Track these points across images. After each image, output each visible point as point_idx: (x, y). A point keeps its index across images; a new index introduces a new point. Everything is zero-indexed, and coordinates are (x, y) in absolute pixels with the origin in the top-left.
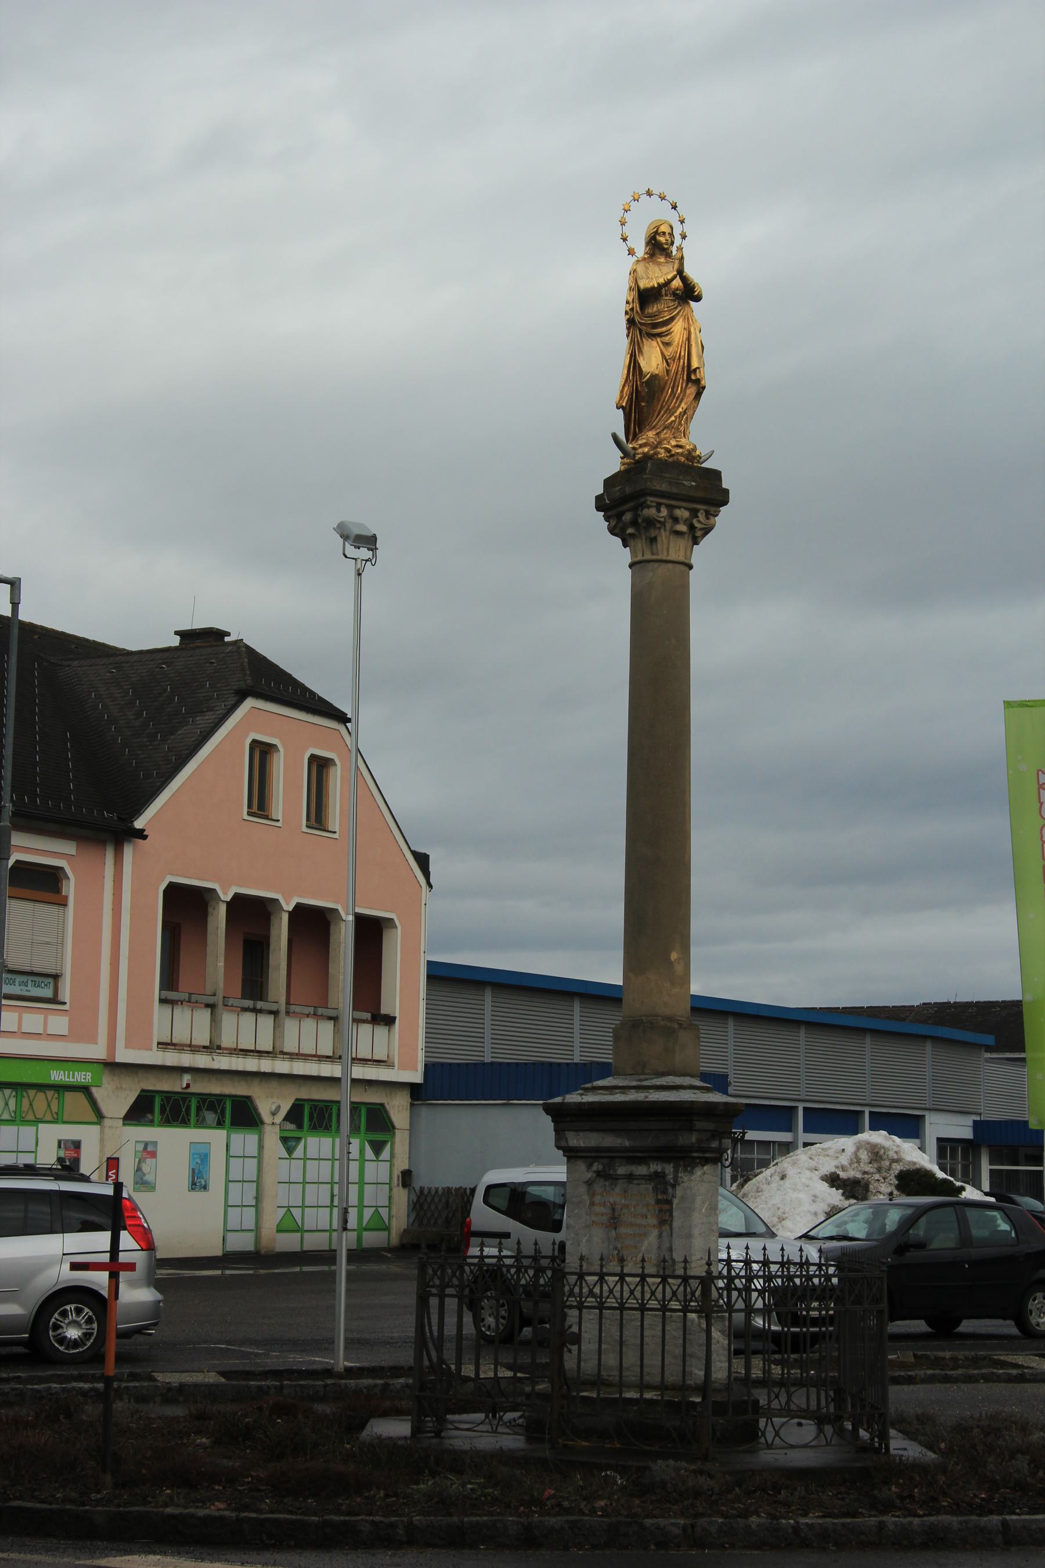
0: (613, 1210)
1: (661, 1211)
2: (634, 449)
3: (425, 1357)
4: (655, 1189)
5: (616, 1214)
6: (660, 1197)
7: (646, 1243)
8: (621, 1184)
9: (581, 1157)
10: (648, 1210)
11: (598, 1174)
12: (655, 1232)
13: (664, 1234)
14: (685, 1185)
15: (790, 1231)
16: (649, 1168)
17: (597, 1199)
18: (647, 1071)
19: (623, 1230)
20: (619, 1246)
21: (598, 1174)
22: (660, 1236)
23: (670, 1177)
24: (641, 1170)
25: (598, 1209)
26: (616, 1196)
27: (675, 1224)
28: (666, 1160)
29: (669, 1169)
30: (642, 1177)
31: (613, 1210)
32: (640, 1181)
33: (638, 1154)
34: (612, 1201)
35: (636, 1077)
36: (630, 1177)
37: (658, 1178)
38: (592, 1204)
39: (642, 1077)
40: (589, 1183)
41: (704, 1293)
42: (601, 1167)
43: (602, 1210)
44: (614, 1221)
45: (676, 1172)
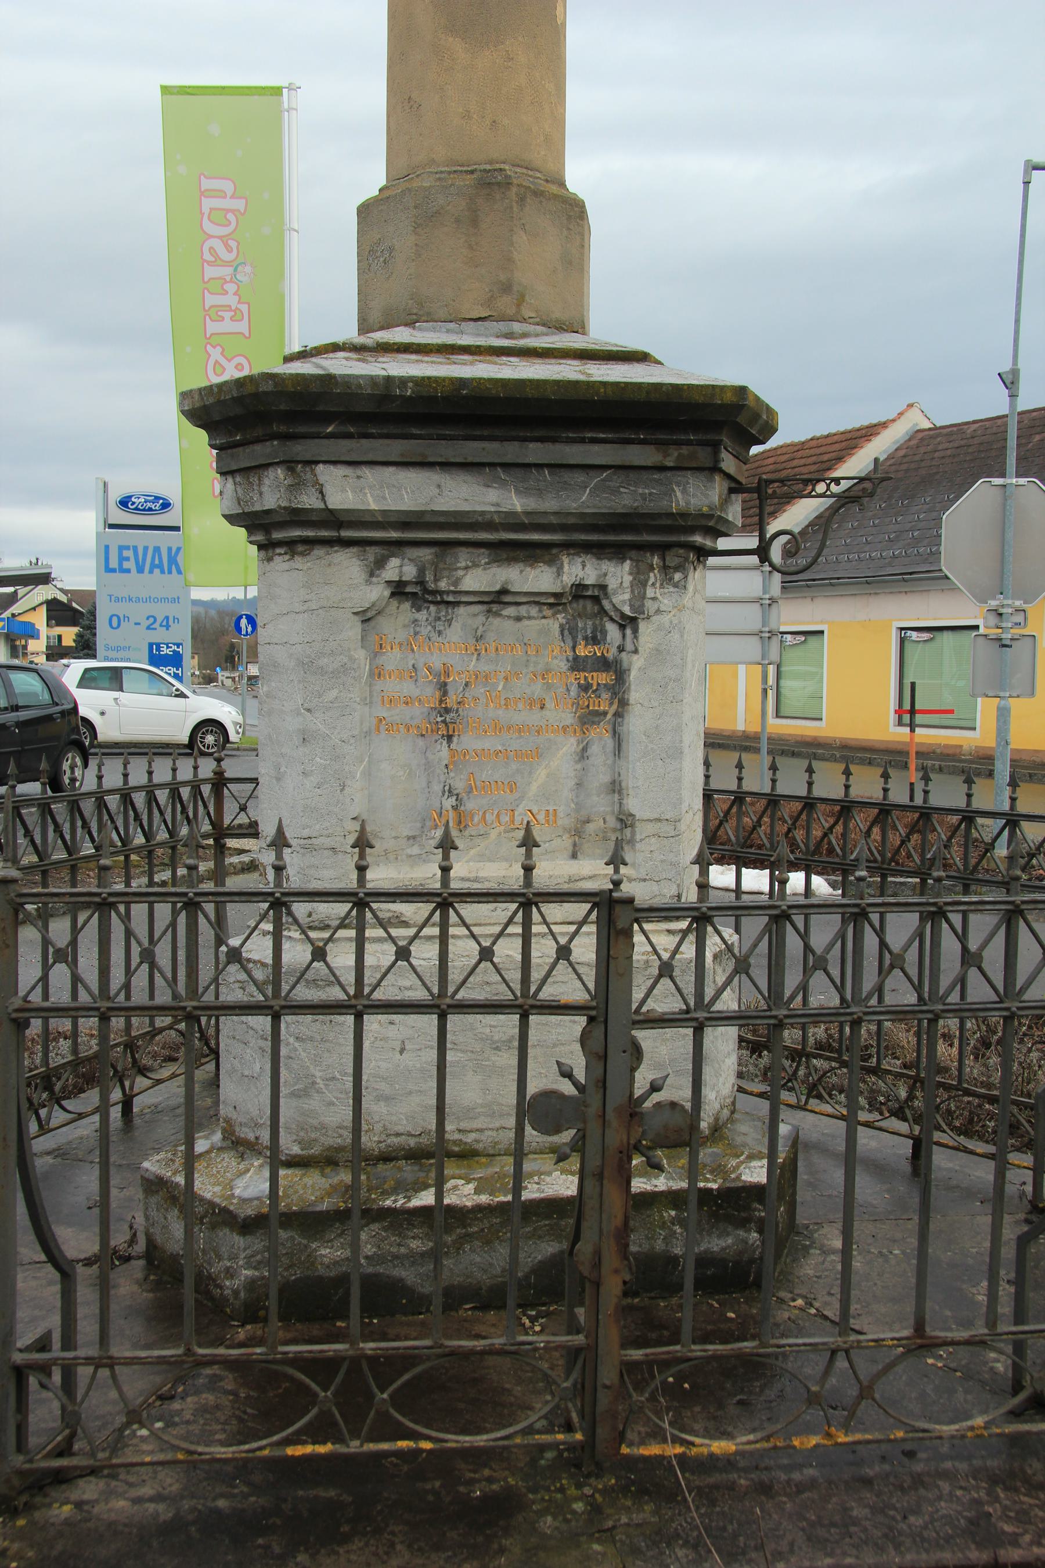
0: (443, 687)
1: (585, 688)
2: (978, 1488)
3: (122, 833)
4: (569, 631)
5: (451, 701)
6: (582, 651)
7: (541, 774)
8: (466, 617)
9: (347, 543)
10: (548, 687)
11: (398, 590)
12: (570, 745)
13: (594, 749)
14: (665, 619)
15: (1031, 1295)
16: (559, 573)
17: (392, 659)
18: (527, 313)
19: (467, 741)
20: (459, 785)
21: (398, 590)
22: (583, 754)
23: (622, 599)
24: (539, 579)
25: (392, 686)
26: (451, 645)
27: (636, 723)
28: (617, 551)
29: (618, 577)
30: (536, 599)
31: (443, 687)
32: (523, 610)
33: (536, 537)
34: (437, 663)
35: (502, 326)
36: (497, 600)
37: (587, 598)
38: (377, 673)
39: (516, 327)
40: (367, 617)
41: (604, 1499)
42: (410, 572)
43: (408, 688)
44: (445, 721)
45: (640, 583)
